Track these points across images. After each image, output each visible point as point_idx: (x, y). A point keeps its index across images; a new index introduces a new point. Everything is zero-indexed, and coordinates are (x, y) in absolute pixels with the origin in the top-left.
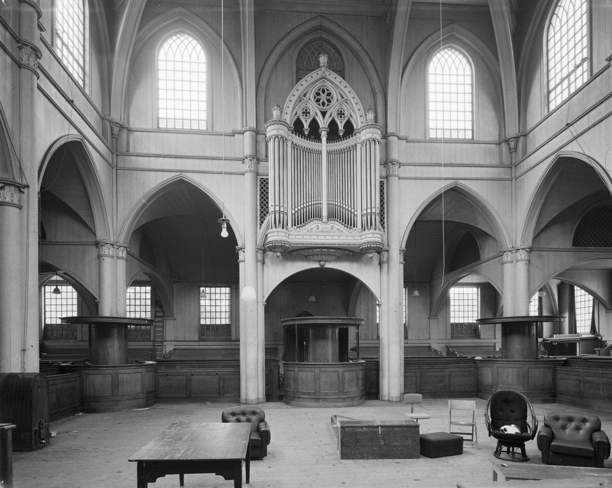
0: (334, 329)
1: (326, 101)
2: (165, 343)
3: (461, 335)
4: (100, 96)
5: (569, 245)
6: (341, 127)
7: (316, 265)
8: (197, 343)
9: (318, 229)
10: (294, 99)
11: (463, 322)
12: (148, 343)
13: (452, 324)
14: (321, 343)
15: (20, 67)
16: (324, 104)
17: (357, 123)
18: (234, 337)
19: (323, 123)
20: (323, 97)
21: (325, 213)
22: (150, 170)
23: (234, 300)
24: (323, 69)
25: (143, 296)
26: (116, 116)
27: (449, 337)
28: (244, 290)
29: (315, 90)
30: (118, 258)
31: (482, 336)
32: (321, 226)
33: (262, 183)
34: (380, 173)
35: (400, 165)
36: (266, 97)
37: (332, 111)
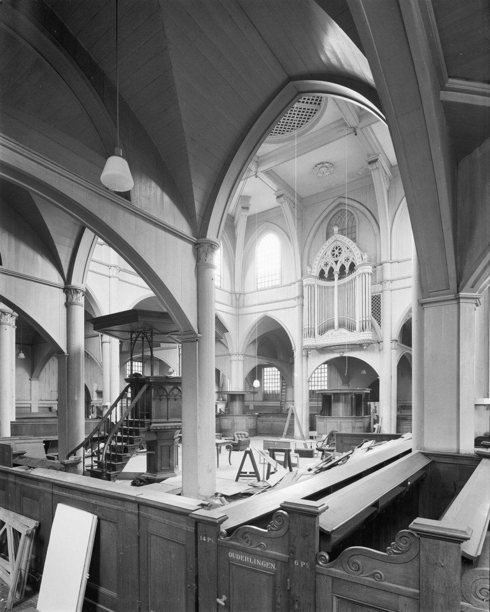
2: (287, 403)
4: (230, 281)
7: (337, 355)
8: (261, 403)
9: (332, 334)
10: (318, 259)
12: (278, 402)
14: (337, 404)
15: (110, 277)
17: (358, 262)
21: (336, 324)
22: (252, 313)
24: (335, 235)
26: (237, 290)
29: (331, 249)
30: (239, 360)
33: (377, 297)
35: (392, 281)
36: (305, 259)
37: (342, 259)
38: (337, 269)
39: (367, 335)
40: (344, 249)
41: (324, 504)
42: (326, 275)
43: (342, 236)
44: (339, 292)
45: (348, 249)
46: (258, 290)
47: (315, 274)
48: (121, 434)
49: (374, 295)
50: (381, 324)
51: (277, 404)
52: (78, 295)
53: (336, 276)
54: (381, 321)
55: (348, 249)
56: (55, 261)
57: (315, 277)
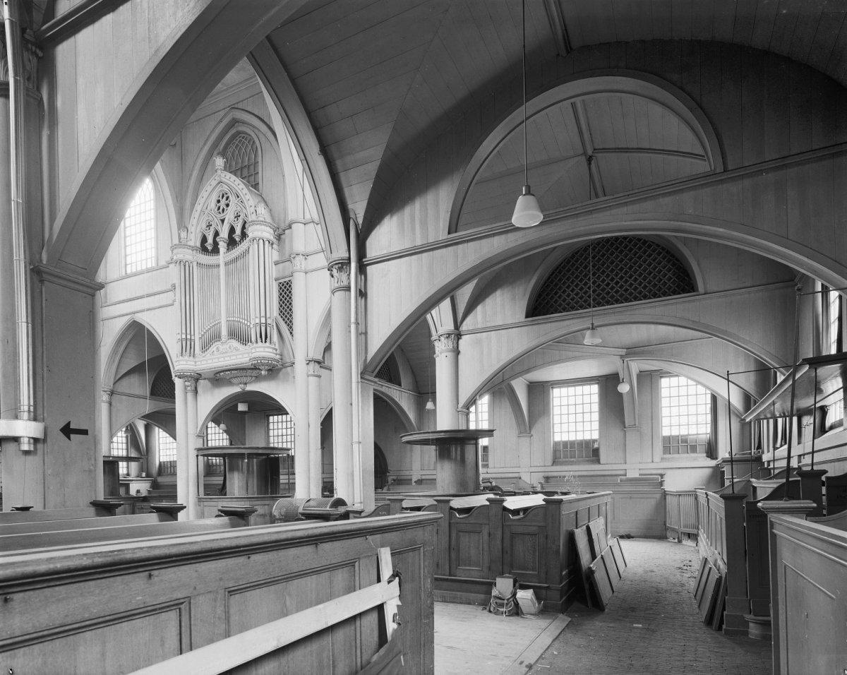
0: (251, 460)
3: (572, 459)
5: (520, 315)
11: (677, 434)
13: (556, 444)
21: (224, 332)
25: (587, 399)
27: (549, 462)
28: (693, 388)
32: (221, 348)
34: (219, 272)
35: (306, 256)
37: (229, 215)
38: (224, 234)
39: (262, 349)
40: (232, 198)
41: (799, 443)
42: (208, 247)
43: (229, 175)
44: (228, 274)
45: (238, 197)
46: (128, 276)
47: (191, 243)
49: (282, 281)
50: (294, 333)
53: (222, 246)
54: (294, 327)
55: (238, 197)
57: (193, 248)
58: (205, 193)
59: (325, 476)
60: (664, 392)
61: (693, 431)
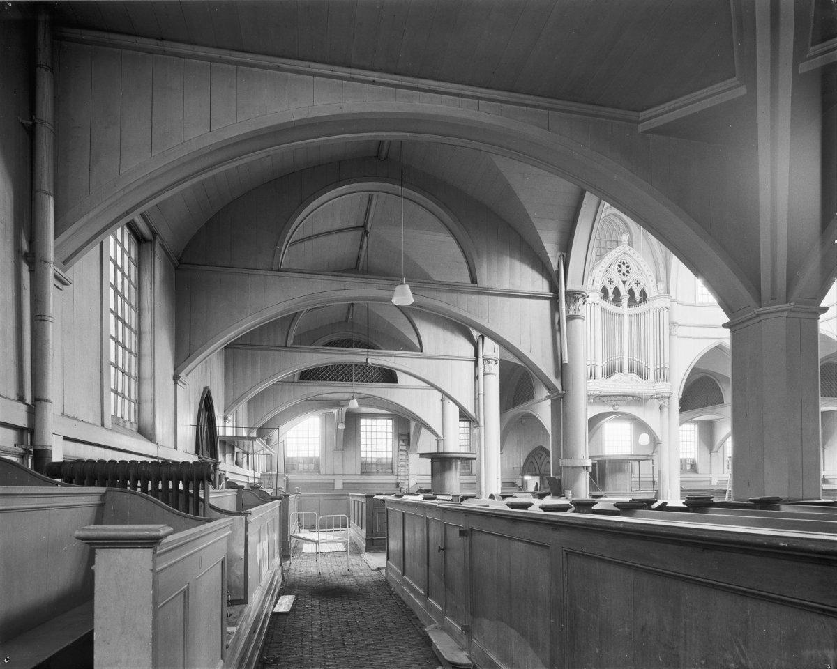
1: (626, 272)
6: (637, 295)
16: (624, 274)
18: (474, 472)
19: (624, 292)
20: (624, 269)
21: (626, 367)
23: (418, 430)
31: (700, 471)
48: (141, 491)
51: (391, 479)
52: (577, 305)
56: (539, 263)
58: (653, 285)
59: (504, 477)
60: (363, 428)
61: (384, 455)
